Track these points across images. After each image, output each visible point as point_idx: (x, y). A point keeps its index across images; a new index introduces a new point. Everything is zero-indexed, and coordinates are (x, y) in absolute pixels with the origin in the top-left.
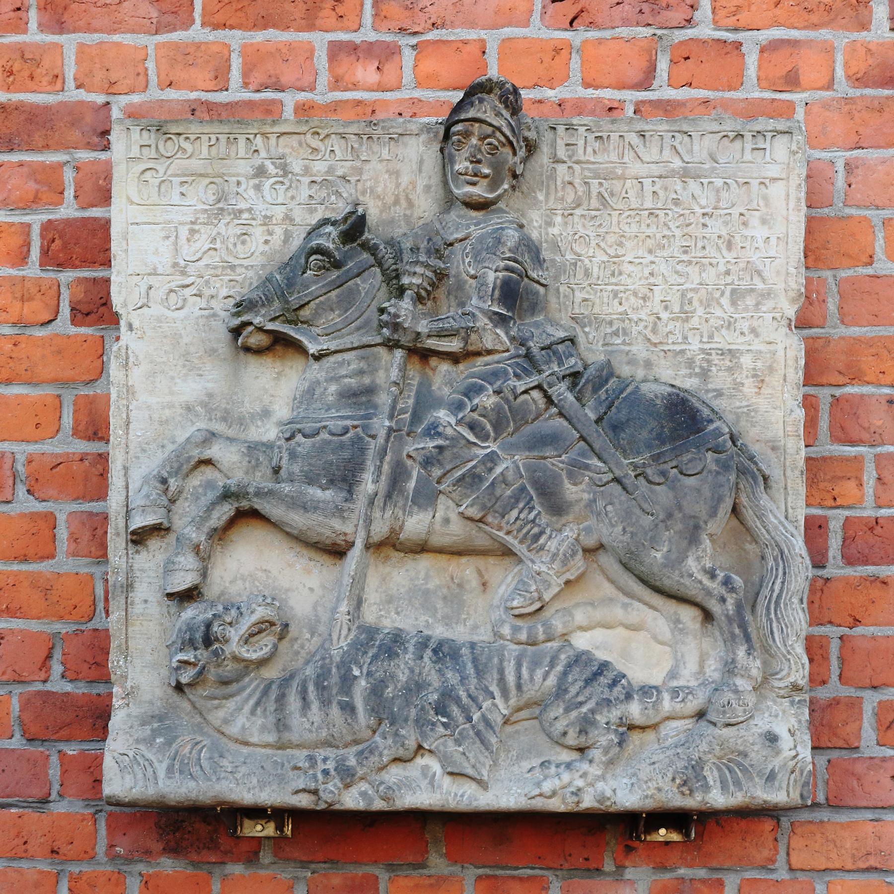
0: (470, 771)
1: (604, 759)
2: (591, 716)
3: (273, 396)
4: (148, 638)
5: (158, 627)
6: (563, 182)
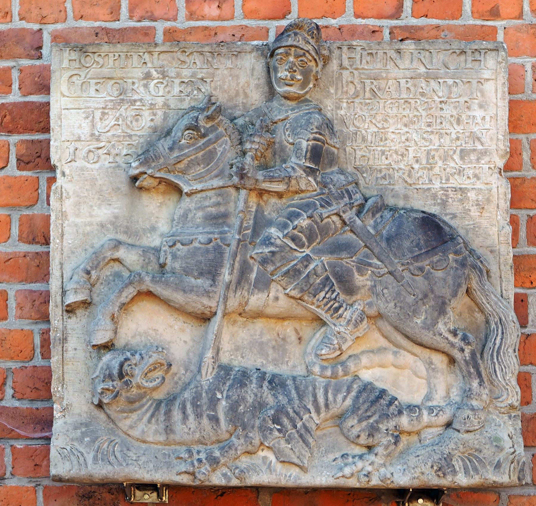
0: (296, 461)
1: (385, 453)
2: (375, 425)
3: (157, 218)
4: (77, 373)
5: (84, 366)
6: (347, 82)
